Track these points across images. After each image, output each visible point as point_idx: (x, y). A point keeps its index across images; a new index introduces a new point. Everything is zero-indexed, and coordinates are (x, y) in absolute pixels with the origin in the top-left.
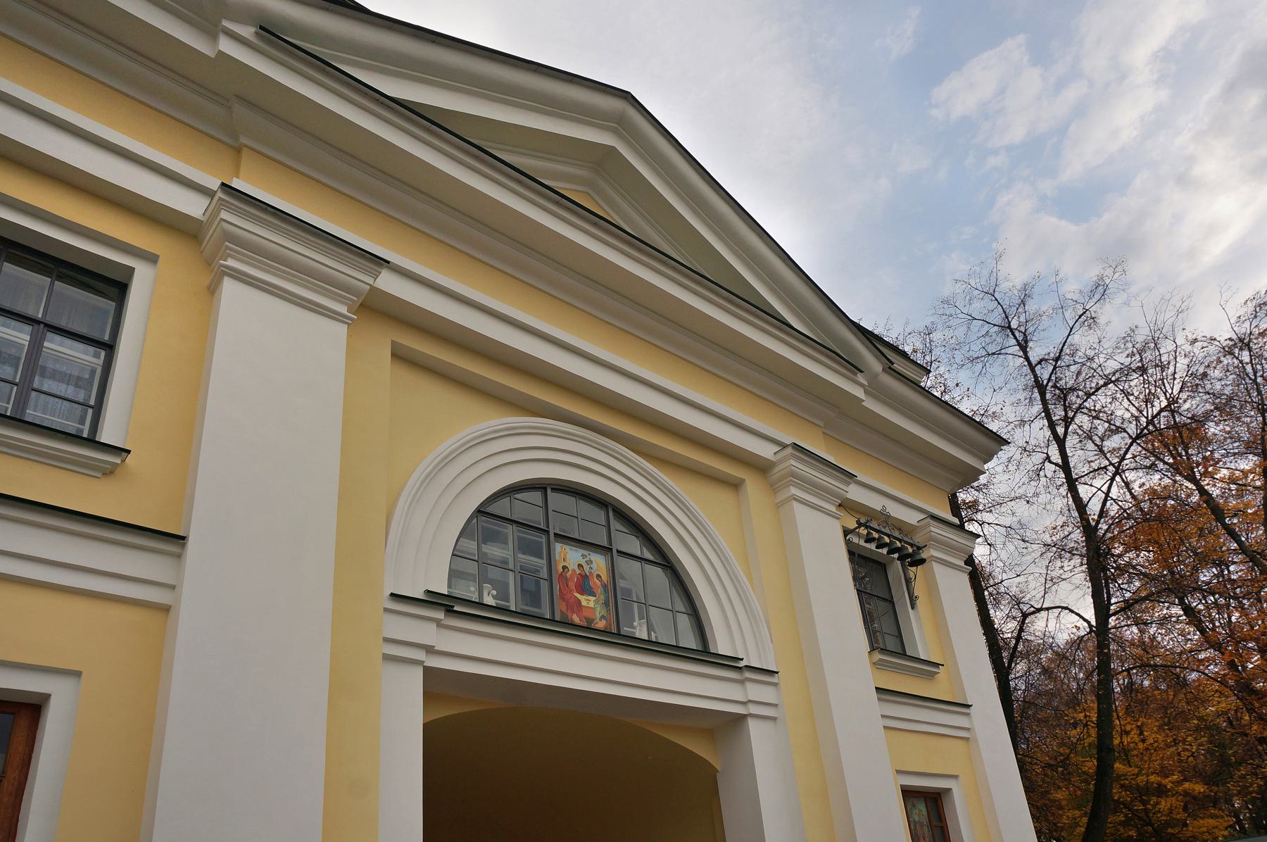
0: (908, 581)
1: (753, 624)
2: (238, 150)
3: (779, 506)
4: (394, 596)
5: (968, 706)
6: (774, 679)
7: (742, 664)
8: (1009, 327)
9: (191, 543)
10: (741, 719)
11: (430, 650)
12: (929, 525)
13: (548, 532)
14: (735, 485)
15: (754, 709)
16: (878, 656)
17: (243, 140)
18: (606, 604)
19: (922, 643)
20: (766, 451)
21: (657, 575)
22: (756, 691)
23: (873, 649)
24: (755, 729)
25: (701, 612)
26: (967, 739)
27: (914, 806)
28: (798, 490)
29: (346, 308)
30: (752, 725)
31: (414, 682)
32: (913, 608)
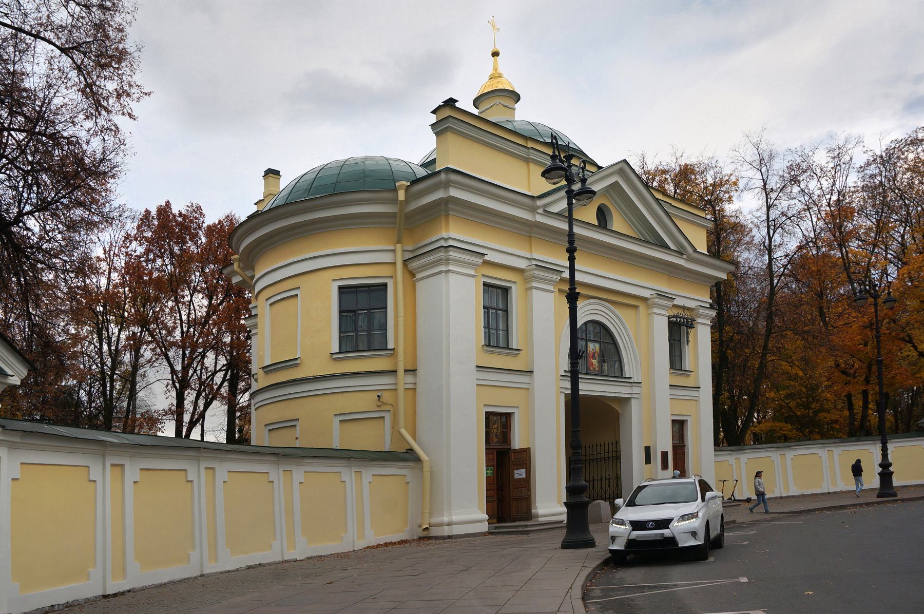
0: (687, 333)
1: (611, 199)
2: (530, 237)
3: (649, 314)
4: (561, 375)
5: (699, 388)
6: (640, 385)
7: (631, 381)
8: (761, 170)
9: (535, 372)
10: (629, 399)
12: (699, 309)
13: (586, 340)
14: (636, 307)
15: (634, 396)
16: (672, 371)
17: (532, 235)
18: (599, 362)
19: (688, 364)
20: (646, 294)
21: (611, 346)
22: (636, 390)
23: (671, 368)
24: (634, 403)
25: (620, 352)
26: (697, 400)
27: (675, 425)
28: (641, 204)
29: (474, 271)
30: (632, 400)
31: (563, 396)
32: (687, 344)
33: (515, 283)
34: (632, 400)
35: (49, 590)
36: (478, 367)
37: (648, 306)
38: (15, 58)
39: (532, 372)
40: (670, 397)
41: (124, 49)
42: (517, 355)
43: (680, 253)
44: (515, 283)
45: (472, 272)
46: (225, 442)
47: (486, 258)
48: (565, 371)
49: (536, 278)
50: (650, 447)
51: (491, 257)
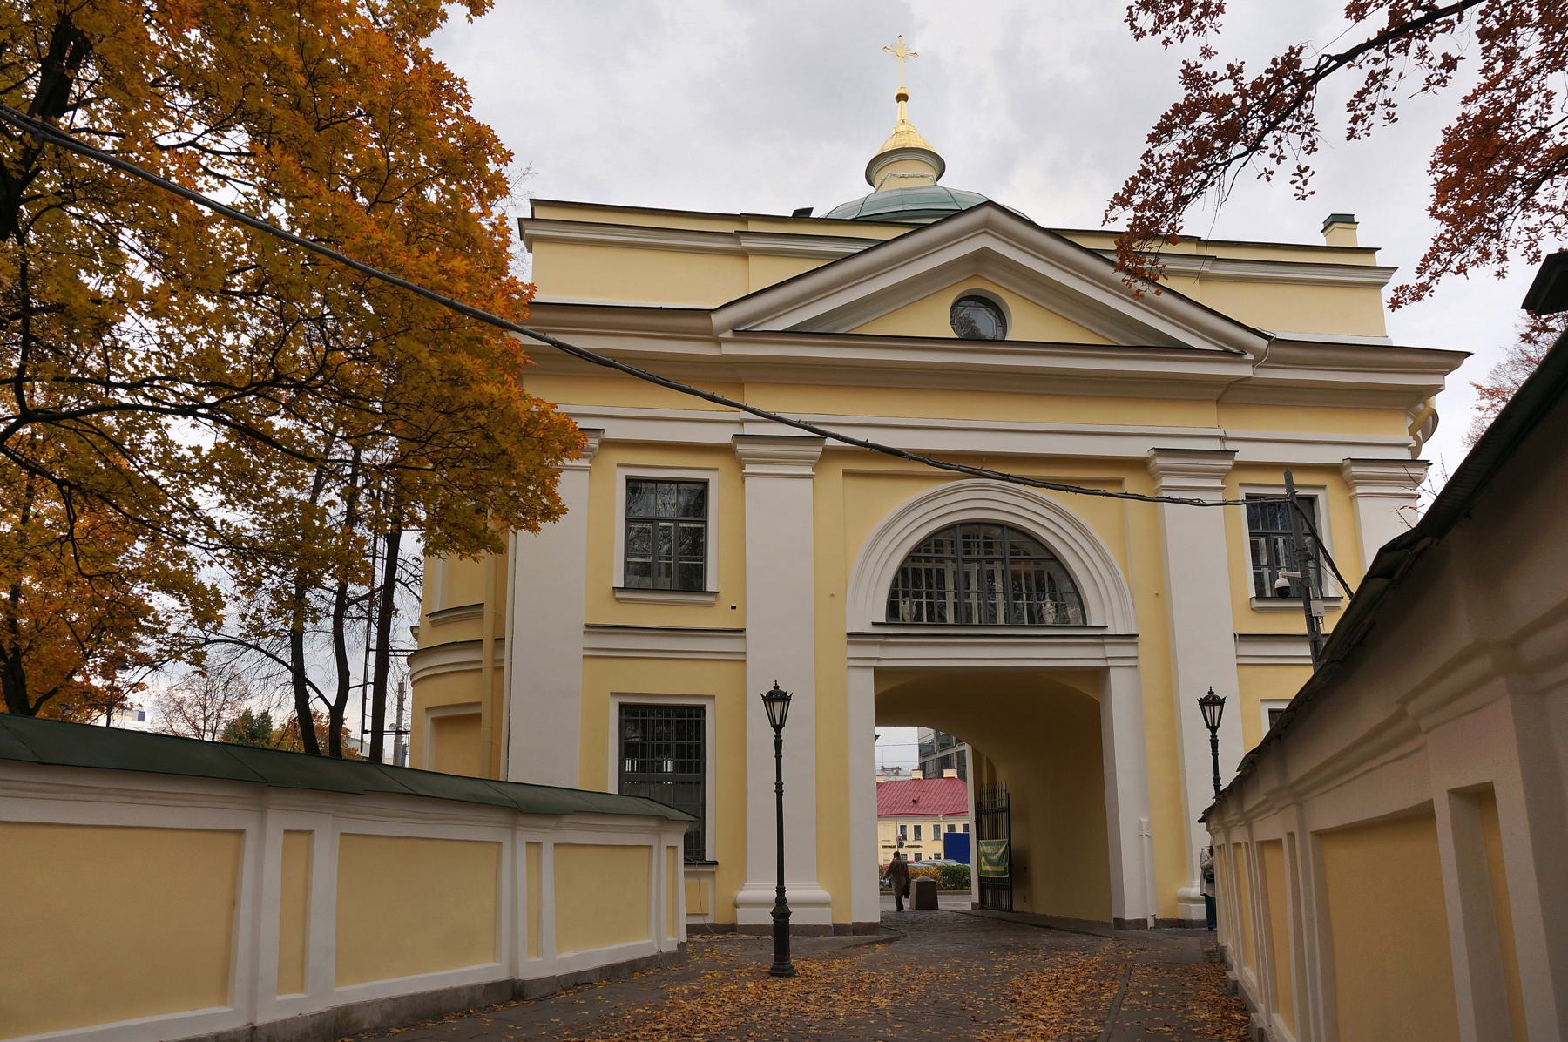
7: (1109, 632)
11: (879, 659)
15: (1111, 663)
33: (1323, 487)
34: (1111, 670)
35: (588, 951)
36: (588, 626)
37: (1151, 475)
38: (120, 390)
39: (742, 631)
40: (1235, 661)
41: (251, 343)
42: (711, 605)
43: (1233, 353)
44: (1323, 487)
45: (808, 471)
46: (303, 750)
47: (1238, 457)
48: (874, 624)
49: (1165, 469)
50: (1491, 784)
51: (1246, 453)
